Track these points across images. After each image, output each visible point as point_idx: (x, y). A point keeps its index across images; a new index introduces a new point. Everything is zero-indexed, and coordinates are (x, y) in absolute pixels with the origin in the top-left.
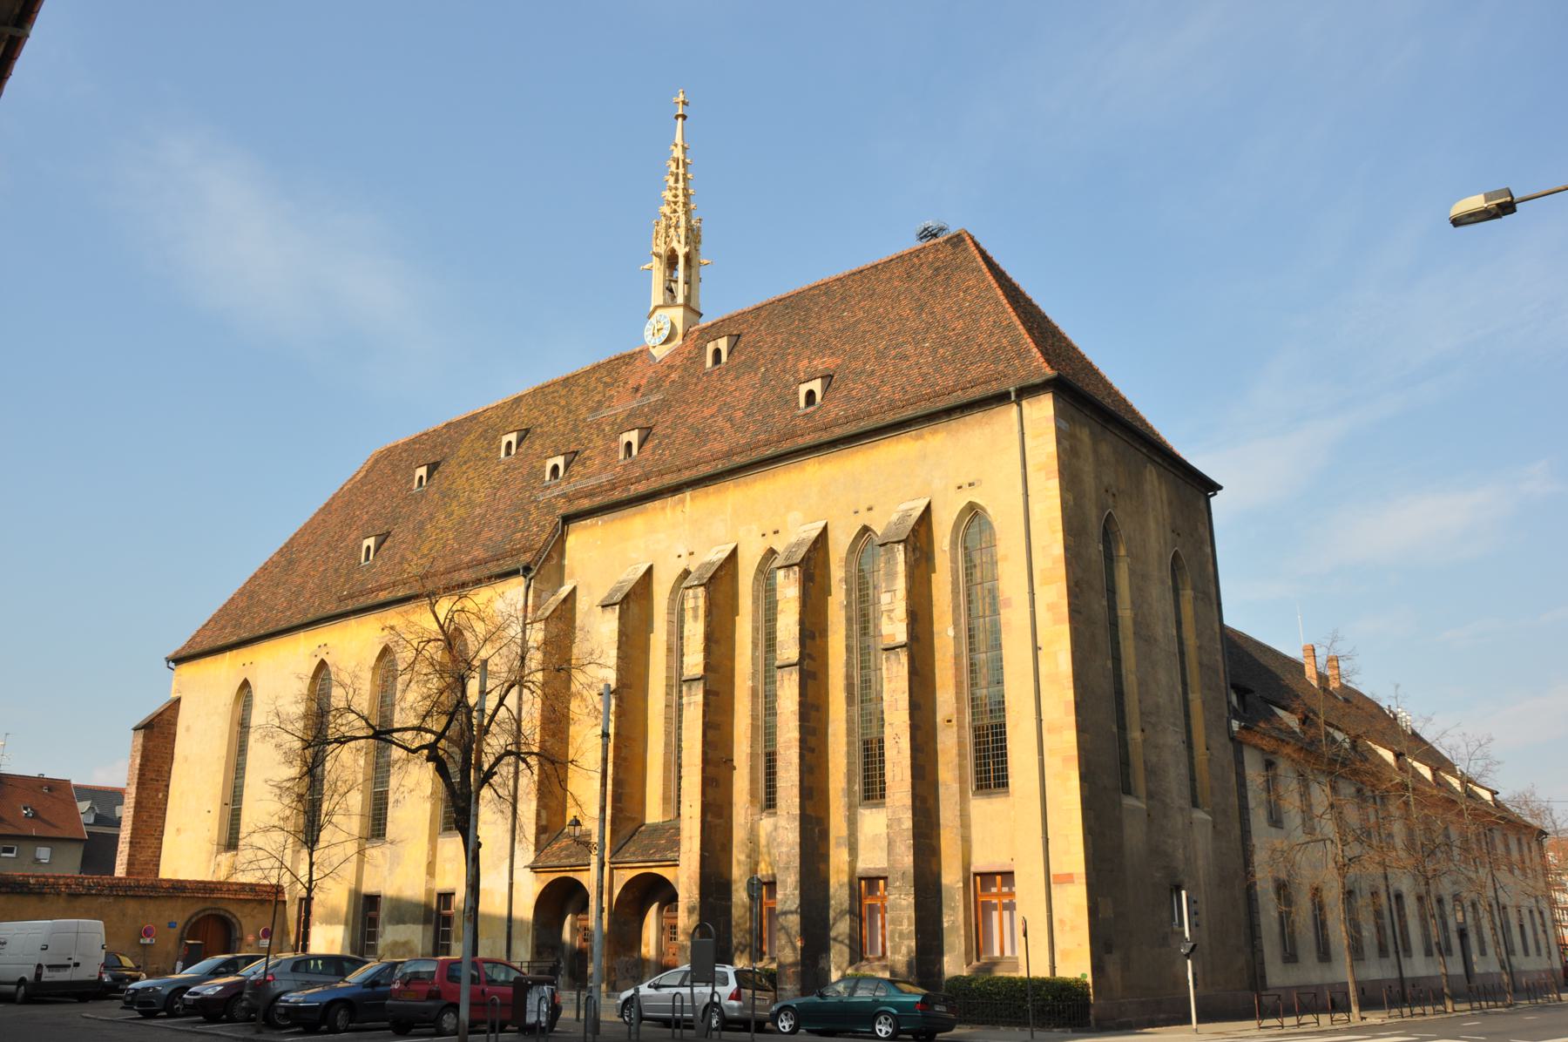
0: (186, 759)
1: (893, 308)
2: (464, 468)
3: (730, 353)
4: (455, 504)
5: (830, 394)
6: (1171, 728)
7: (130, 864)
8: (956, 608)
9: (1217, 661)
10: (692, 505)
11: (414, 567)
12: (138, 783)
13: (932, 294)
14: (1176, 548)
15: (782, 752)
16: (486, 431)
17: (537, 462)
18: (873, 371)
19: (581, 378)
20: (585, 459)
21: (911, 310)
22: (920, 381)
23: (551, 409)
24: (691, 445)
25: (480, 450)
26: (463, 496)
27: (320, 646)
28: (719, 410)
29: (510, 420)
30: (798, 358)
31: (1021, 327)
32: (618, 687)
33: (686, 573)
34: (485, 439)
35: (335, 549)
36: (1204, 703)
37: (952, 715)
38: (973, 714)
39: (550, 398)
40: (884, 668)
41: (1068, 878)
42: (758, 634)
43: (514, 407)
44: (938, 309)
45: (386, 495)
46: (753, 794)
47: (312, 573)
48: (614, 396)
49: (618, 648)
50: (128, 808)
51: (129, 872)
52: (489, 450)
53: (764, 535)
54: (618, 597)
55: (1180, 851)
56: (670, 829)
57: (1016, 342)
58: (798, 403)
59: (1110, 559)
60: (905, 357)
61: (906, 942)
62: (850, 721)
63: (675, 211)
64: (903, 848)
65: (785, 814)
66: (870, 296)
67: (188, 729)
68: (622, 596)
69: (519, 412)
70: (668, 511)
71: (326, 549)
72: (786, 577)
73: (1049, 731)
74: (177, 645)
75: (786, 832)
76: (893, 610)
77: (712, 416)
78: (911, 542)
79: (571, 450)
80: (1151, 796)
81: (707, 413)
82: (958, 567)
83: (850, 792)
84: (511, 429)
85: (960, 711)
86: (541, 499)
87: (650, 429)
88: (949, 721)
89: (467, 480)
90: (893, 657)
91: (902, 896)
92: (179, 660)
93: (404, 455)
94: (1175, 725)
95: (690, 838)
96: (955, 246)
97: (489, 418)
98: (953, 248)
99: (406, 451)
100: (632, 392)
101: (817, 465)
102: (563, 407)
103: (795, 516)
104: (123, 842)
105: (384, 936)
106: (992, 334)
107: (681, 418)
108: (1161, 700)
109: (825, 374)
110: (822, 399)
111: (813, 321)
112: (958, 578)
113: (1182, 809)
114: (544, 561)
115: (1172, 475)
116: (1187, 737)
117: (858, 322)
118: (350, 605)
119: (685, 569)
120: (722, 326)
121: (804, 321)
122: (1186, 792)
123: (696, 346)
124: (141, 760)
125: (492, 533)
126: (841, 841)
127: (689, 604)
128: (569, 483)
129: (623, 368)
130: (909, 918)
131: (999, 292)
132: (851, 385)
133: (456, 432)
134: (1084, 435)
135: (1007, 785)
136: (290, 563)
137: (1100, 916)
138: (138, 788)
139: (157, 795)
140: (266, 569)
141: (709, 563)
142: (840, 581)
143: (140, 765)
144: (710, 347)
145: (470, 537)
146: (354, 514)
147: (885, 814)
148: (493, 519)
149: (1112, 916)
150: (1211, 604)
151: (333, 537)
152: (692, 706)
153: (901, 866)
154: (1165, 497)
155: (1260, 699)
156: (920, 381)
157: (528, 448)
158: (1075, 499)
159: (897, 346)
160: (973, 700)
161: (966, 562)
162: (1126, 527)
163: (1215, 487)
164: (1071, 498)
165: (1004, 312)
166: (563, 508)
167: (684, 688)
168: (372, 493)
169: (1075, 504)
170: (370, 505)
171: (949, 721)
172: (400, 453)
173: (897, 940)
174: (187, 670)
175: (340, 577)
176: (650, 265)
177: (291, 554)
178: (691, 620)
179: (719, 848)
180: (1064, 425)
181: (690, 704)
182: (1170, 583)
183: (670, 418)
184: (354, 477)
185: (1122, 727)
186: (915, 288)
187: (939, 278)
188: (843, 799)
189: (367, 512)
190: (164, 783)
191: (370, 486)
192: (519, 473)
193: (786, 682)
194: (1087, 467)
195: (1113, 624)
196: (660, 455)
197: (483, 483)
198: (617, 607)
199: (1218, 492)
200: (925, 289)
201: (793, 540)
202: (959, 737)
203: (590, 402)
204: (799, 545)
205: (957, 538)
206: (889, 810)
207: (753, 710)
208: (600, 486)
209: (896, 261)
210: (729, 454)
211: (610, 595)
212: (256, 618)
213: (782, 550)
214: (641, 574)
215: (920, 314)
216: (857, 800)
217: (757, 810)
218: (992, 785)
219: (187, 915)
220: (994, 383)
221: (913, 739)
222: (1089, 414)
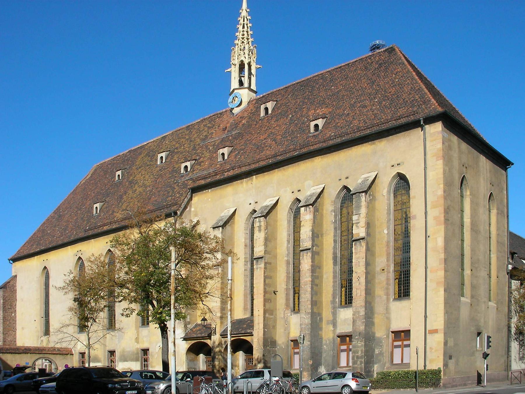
0: (22, 300)
1: (358, 84)
2: (140, 170)
4: (136, 186)
6: (484, 269)
9: (505, 240)
11: (119, 215)
13: (379, 76)
15: (303, 286)
16: (149, 152)
17: (176, 165)
18: (348, 114)
19: (196, 125)
20: (200, 162)
21: (367, 84)
23: (181, 141)
24: (255, 153)
25: (146, 161)
26: (141, 183)
27: (78, 251)
28: (269, 136)
29: (161, 147)
30: (309, 110)
31: (425, 90)
33: (255, 211)
34: (149, 156)
35: (80, 209)
36: (498, 258)
37: (385, 267)
39: (180, 135)
41: (436, 331)
42: (290, 237)
43: (162, 141)
44: (381, 83)
45: (102, 184)
46: (287, 305)
47: (70, 220)
48: (213, 133)
52: (151, 161)
53: (293, 192)
54: (221, 223)
55: (483, 319)
56: (248, 321)
57: (422, 97)
58: (310, 131)
60: (365, 107)
61: (360, 360)
62: (335, 272)
63: (243, 42)
64: (360, 323)
65: (304, 312)
67: (22, 288)
68: (223, 223)
69: (165, 143)
70: (244, 184)
71: (76, 210)
72: (306, 210)
73: (431, 272)
74: (13, 253)
75: (304, 319)
76: (358, 223)
79: (193, 159)
80: (472, 297)
83: (333, 302)
84: (162, 151)
85: (388, 266)
86: (180, 181)
88: (384, 270)
89: (142, 175)
91: (359, 342)
92: (15, 260)
93: (110, 166)
94: (485, 268)
95: (258, 324)
96: (390, 53)
97: (150, 147)
98: (389, 54)
101: (320, 159)
102: (188, 139)
103: (309, 182)
105: (118, 366)
106: (410, 94)
107: (249, 141)
108: (480, 258)
111: (315, 92)
113: (485, 302)
117: (340, 91)
118: (91, 233)
119: (253, 210)
120: (267, 97)
123: (254, 107)
125: (156, 198)
126: (330, 322)
127: (256, 225)
128: (193, 174)
129: (217, 119)
130: (362, 351)
132: (337, 121)
133: (134, 154)
135: (409, 295)
136: (59, 216)
140: (49, 220)
141: (266, 206)
142: (331, 211)
143: (3, 303)
144: (263, 107)
146: (88, 194)
147: (352, 310)
150: (504, 216)
152: (259, 270)
153: (358, 330)
154: (488, 168)
157: (171, 159)
159: (361, 101)
164: (448, 169)
166: (191, 185)
167: (255, 262)
169: (449, 172)
170: (95, 189)
171: (384, 270)
173: (356, 359)
174: (18, 264)
175: (84, 221)
176: (230, 69)
177: (60, 213)
178: (257, 232)
181: (258, 268)
183: (243, 141)
185: (463, 269)
186: (369, 74)
193: (305, 257)
197: (150, 176)
198: (221, 228)
201: (309, 193)
203: (201, 136)
204: (311, 196)
205: (390, 189)
206: (354, 308)
207: (287, 270)
208: (209, 174)
210: (275, 156)
211: (217, 223)
212: (47, 241)
213: (303, 199)
218: (402, 296)
220: (412, 116)
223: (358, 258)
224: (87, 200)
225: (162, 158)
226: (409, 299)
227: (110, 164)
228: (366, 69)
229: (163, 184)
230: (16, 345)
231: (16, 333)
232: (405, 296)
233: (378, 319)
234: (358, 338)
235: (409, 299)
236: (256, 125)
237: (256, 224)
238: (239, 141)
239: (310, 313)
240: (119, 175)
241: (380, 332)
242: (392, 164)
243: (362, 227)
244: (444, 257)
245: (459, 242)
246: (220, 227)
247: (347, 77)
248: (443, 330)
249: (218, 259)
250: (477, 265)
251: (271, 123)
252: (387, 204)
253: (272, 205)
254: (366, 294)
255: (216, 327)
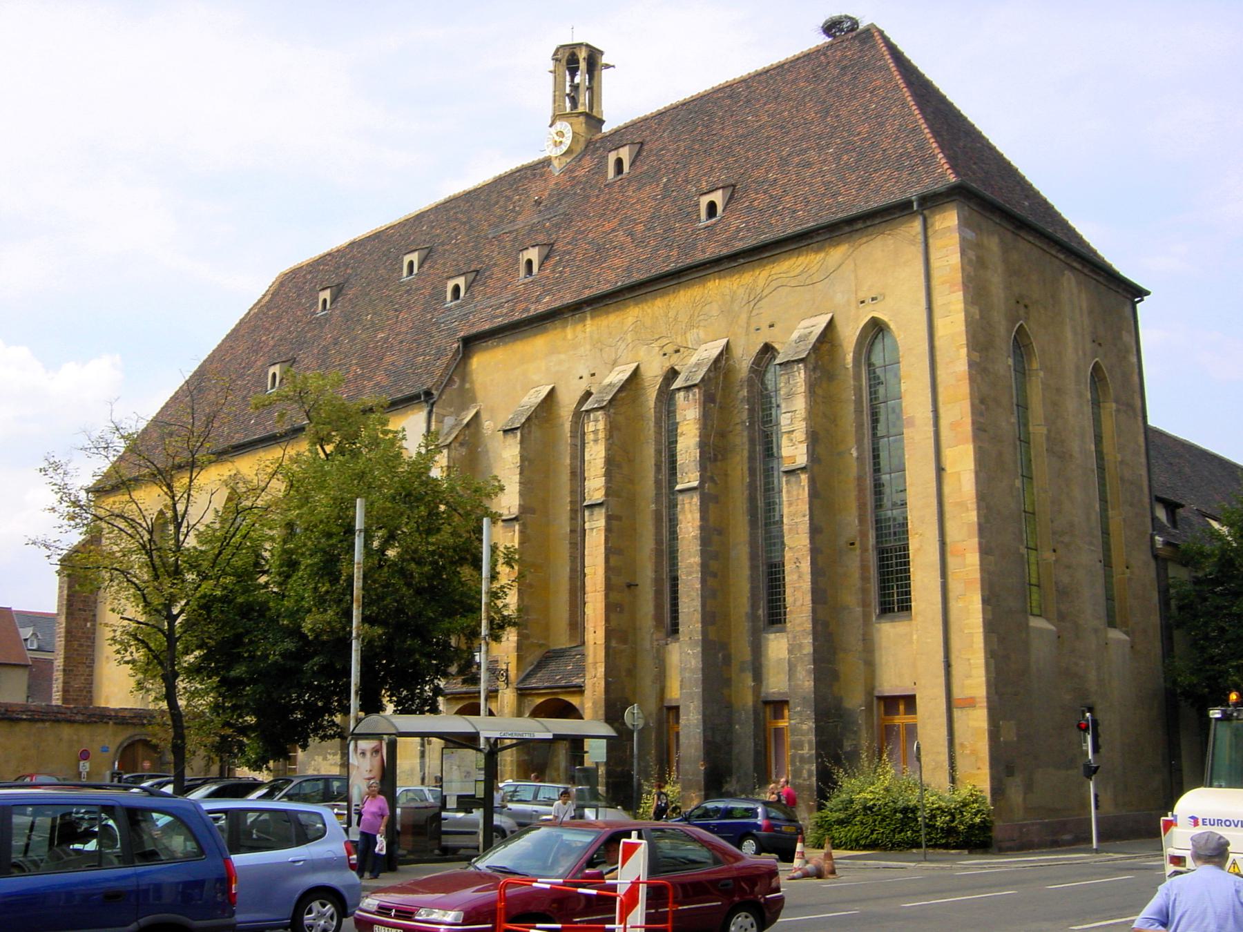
3: (632, 164)
5: (732, 206)
7: (65, 691)
8: (860, 426)
10: (591, 328)
12: (67, 613)
14: (1097, 359)
18: (775, 180)
22: (822, 190)
24: (591, 262)
32: (524, 509)
33: (588, 394)
38: (877, 537)
40: (784, 491)
41: (970, 703)
44: (844, 112)
49: (520, 474)
50: (59, 637)
51: (65, 700)
56: (576, 655)
57: (921, 147)
58: (699, 216)
59: (1022, 372)
61: (807, 767)
66: (776, 98)
70: (589, 322)
72: (687, 398)
76: (793, 431)
77: (613, 230)
78: (812, 361)
79: (472, 269)
81: (608, 227)
82: (861, 385)
83: (753, 617)
85: (863, 535)
87: (552, 245)
88: (852, 544)
90: (793, 479)
93: (309, 277)
94: (1091, 543)
95: (595, 663)
99: (310, 272)
100: (534, 206)
102: (465, 223)
104: (57, 670)
106: (897, 139)
109: (728, 183)
110: (723, 211)
111: (717, 127)
112: (861, 396)
113: (1096, 631)
114: (445, 386)
115: (1094, 282)
116: (1104, 555)
121: (707, 127)
122: (1102, 611)
124: (68, 591)
127: (590, 427)
130: (810, 742)
131: (906, 93)
133: (359, 252)
134: (993, 244)
137: (1002, 739)
138: (67, 618)
139: (86, 625)
140: (177, 398)
145: (373, 361)
146: (260, 339)
148: (395, 343)
149: (1015, 739)
151: (240, 364)
154: (1084, 305)
155: (1196, 512)
156: (822, 190)
158: (981, 311)
160: (877, 522)
161: (870, 380)
162: (1039, 340)
163: (1140, 293)
164: (977, 312)
165: (911, 114)
167: (587, 513)
168: (277, 317)
169: (982, 317)
171: (852, 544)
172: (304, 276)
179: (624, 674)
180: (970, 235)
181: (593, 529)
182: (1089, 396)
184: (260, 301)
187: (846, 79)
188: (746, 624)
189: (273, 338)
190: (92, 613)
191: (276, 310)
192: (421, 294)
194: (996, 280)
195: (1024, 441)
196: (561, 272)
199: (1145, 298)
200: (831, 90)
202: (862, 560)
206: (790, 636)
209: (802, 60)
214: (543, 396)
215: (826, 118)
216: (761, 624)
217: (662, 635)
219: (120, 739)
221: (814, 563)
222: (998, 221)
223: (794, 514)
224: (257, 354)
225: (411, 264)
226: (910, 618)
227: (310, 272)
228: (815, 77)
229: (411, 325)
230: (91, 700)
231: (92, 671)
232: (903, 610)
233: (850, 666)
234: (800, 711)
235: (910, 618)
236: (597, 196)
237: (588, 426)
238: (563, 233)
239: (700, 643)
240: (325, 301)
241: (855, 700)
242: (861, 296)
243: (801, 442)
244: (978, 518)
245: (1017, 481)
246: (517, 429)
247: (778, 96)
248: (985, 700)
249: (113, 610)
250: (1066, 539)
251: (626, 194)
252: (854, 389)
253: (622, 382)
254: (813, 601)
255: (507, 670)
